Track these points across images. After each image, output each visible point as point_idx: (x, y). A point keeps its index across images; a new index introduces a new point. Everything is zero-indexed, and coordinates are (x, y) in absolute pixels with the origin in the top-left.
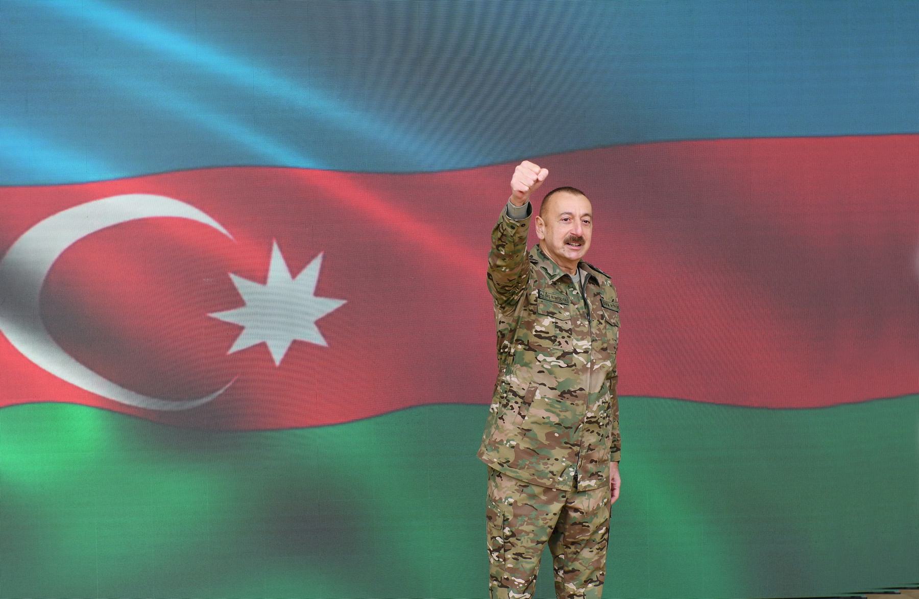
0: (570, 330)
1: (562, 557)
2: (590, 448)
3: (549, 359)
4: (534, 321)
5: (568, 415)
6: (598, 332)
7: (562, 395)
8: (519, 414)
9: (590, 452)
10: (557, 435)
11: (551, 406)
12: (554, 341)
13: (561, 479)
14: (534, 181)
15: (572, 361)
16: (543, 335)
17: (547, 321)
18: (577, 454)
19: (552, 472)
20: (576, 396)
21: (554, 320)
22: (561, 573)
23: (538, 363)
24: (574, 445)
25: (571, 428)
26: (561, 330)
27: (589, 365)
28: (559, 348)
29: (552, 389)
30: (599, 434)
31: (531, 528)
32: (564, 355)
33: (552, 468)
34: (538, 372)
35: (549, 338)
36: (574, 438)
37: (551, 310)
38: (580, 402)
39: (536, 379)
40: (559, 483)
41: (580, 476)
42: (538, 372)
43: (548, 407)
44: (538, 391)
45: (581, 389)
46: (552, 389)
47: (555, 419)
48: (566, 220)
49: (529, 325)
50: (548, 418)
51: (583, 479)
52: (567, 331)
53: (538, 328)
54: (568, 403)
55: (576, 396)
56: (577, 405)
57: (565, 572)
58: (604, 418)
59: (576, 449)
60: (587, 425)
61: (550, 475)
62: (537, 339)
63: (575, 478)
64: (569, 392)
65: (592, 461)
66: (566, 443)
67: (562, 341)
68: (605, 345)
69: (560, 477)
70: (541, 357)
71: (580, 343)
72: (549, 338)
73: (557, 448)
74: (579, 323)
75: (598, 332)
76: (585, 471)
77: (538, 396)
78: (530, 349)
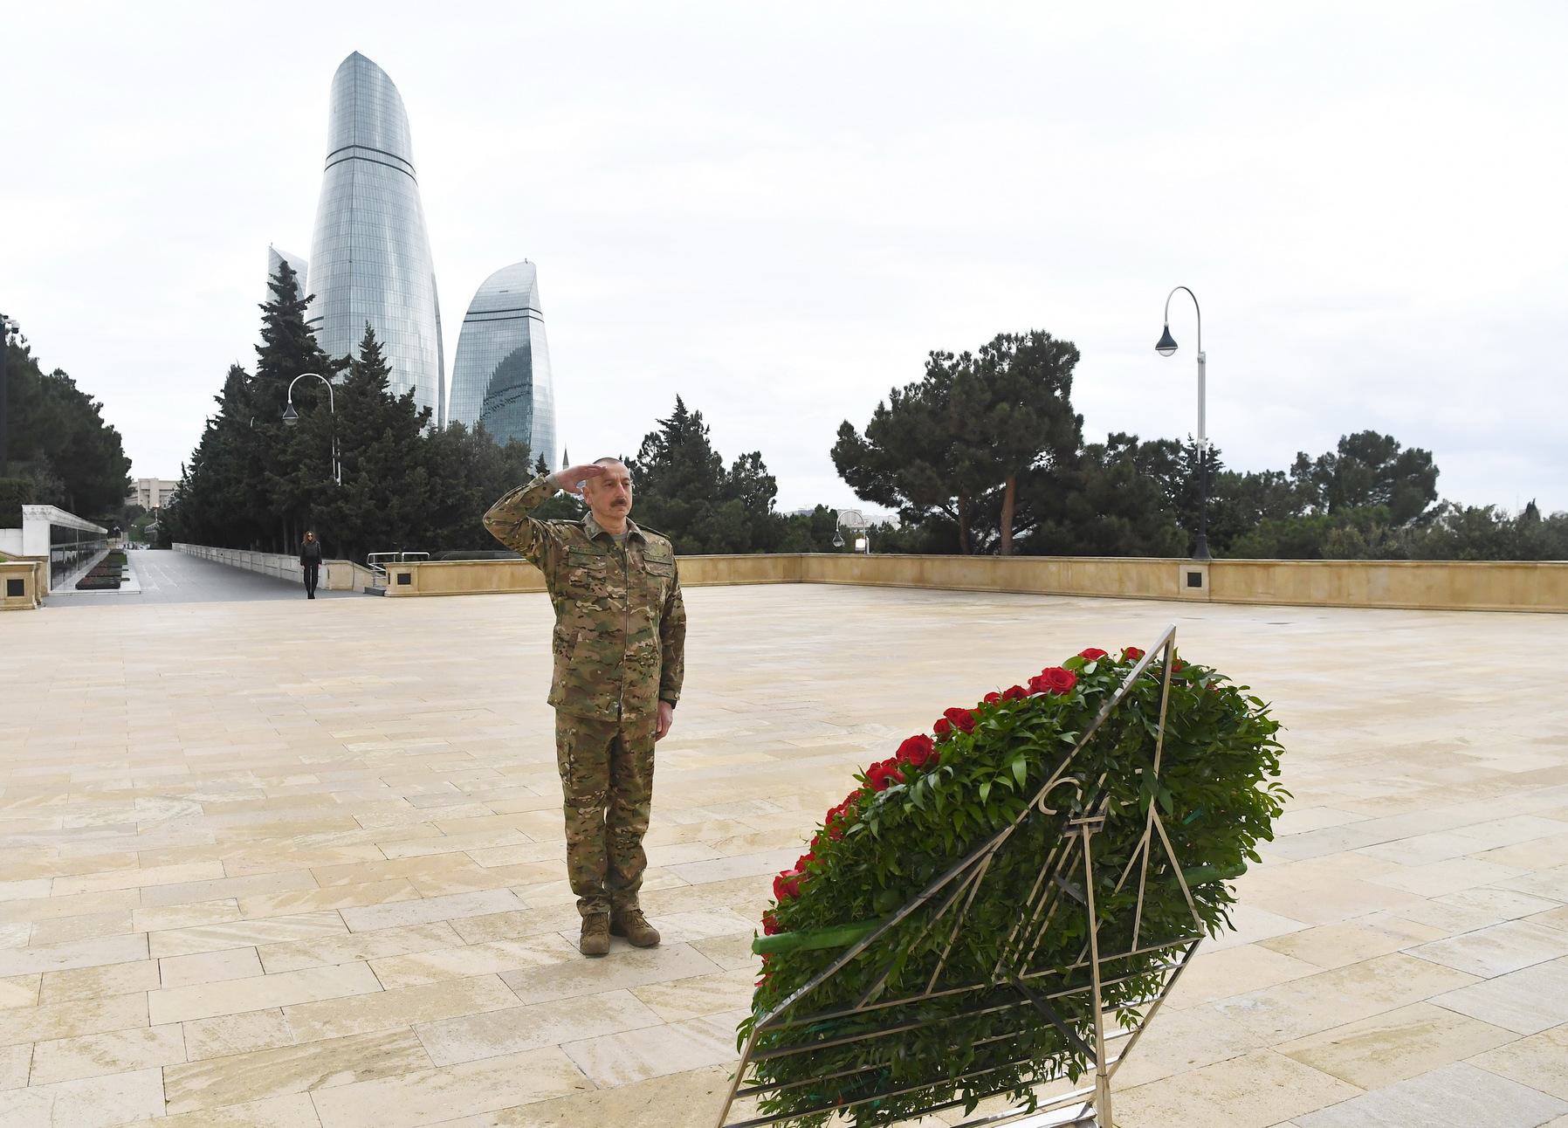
0: (604, 578)
1: (618, 776)
2: (632, 684)
3: (586, 604)
4: (569, 573)
5: (608, 652)
6: (636, 581)
7: (600, 636)
8: (567, 656)
9: (632, 688)
10: (599, 672)
11: (591, 645)
12: (587, 589)
13: (607, 712)
14: (841, 476)
15: (607, 605)
16: (577, 584)
17: (579, 572)
18: (620, 688)
19: (598, 705)
20: (614, 637)
21: (586, 570)
22: (616, 789)
23: (577, 609)
24: (616, 680)
25: (611, 664)
26: (594, 578)
27: (625, 609)
28: (593, 594)
29: (591, 631)
30: (641, 673)
31: (590, 755)
32: (598, 601)
33: (597, 702)
34: (1259, 861)
35: (583, 586)
36: (615, 675)
37: (584, 561)
38: (619, 642)
39: (577, 624)
40: (606, 715)
41: (623, 709)
42: (1259, 861)
43: (590, 648)
44: (580, 635)
45: (618, 630)
46: (591, 631)
47: (596, 657)
48: (610, 485)
49: (566, 578)
50: (590, 657)
51: (625, 713)
52: (599, 579)
53: (573, 578)
54: (607, 642)
55: (614, 637)
56: (615, 644)
57: (619, 790)
58: (647, 659)
59: (617, 683)
60: (628, 663)
61: (597, 708)
62: (573, 589)
63: (620, 709)
64: (607, 633)
65: (634, 697)
66: (609, 679)
67: (596, 588)
68: (645, 593)
69: (1068, 929)
70: (579, 604)
71: (616, 590)
72: (583, 586)
73: (128, 475)
74: (616, 572)
75: (636, 581)
76: (627, 702)
77: (580, 639)
78: (569, 598)
